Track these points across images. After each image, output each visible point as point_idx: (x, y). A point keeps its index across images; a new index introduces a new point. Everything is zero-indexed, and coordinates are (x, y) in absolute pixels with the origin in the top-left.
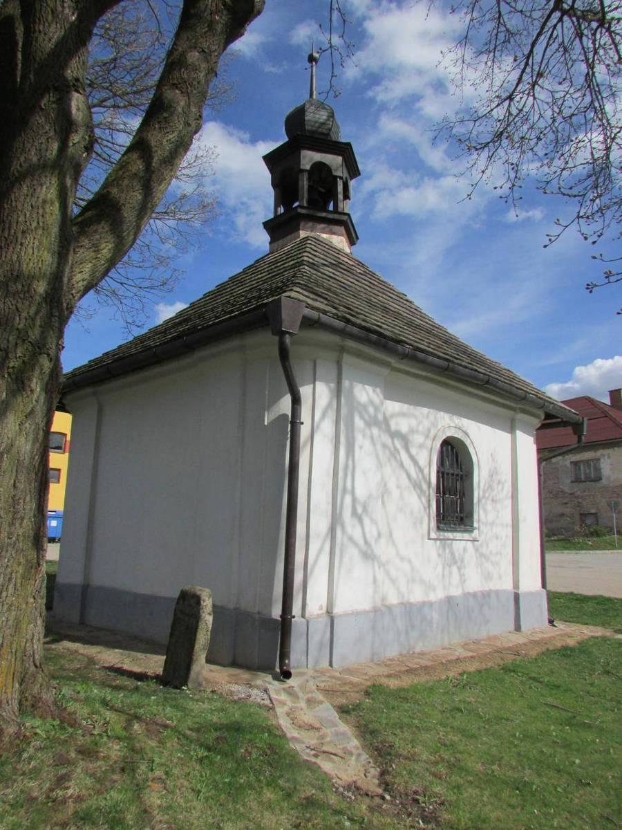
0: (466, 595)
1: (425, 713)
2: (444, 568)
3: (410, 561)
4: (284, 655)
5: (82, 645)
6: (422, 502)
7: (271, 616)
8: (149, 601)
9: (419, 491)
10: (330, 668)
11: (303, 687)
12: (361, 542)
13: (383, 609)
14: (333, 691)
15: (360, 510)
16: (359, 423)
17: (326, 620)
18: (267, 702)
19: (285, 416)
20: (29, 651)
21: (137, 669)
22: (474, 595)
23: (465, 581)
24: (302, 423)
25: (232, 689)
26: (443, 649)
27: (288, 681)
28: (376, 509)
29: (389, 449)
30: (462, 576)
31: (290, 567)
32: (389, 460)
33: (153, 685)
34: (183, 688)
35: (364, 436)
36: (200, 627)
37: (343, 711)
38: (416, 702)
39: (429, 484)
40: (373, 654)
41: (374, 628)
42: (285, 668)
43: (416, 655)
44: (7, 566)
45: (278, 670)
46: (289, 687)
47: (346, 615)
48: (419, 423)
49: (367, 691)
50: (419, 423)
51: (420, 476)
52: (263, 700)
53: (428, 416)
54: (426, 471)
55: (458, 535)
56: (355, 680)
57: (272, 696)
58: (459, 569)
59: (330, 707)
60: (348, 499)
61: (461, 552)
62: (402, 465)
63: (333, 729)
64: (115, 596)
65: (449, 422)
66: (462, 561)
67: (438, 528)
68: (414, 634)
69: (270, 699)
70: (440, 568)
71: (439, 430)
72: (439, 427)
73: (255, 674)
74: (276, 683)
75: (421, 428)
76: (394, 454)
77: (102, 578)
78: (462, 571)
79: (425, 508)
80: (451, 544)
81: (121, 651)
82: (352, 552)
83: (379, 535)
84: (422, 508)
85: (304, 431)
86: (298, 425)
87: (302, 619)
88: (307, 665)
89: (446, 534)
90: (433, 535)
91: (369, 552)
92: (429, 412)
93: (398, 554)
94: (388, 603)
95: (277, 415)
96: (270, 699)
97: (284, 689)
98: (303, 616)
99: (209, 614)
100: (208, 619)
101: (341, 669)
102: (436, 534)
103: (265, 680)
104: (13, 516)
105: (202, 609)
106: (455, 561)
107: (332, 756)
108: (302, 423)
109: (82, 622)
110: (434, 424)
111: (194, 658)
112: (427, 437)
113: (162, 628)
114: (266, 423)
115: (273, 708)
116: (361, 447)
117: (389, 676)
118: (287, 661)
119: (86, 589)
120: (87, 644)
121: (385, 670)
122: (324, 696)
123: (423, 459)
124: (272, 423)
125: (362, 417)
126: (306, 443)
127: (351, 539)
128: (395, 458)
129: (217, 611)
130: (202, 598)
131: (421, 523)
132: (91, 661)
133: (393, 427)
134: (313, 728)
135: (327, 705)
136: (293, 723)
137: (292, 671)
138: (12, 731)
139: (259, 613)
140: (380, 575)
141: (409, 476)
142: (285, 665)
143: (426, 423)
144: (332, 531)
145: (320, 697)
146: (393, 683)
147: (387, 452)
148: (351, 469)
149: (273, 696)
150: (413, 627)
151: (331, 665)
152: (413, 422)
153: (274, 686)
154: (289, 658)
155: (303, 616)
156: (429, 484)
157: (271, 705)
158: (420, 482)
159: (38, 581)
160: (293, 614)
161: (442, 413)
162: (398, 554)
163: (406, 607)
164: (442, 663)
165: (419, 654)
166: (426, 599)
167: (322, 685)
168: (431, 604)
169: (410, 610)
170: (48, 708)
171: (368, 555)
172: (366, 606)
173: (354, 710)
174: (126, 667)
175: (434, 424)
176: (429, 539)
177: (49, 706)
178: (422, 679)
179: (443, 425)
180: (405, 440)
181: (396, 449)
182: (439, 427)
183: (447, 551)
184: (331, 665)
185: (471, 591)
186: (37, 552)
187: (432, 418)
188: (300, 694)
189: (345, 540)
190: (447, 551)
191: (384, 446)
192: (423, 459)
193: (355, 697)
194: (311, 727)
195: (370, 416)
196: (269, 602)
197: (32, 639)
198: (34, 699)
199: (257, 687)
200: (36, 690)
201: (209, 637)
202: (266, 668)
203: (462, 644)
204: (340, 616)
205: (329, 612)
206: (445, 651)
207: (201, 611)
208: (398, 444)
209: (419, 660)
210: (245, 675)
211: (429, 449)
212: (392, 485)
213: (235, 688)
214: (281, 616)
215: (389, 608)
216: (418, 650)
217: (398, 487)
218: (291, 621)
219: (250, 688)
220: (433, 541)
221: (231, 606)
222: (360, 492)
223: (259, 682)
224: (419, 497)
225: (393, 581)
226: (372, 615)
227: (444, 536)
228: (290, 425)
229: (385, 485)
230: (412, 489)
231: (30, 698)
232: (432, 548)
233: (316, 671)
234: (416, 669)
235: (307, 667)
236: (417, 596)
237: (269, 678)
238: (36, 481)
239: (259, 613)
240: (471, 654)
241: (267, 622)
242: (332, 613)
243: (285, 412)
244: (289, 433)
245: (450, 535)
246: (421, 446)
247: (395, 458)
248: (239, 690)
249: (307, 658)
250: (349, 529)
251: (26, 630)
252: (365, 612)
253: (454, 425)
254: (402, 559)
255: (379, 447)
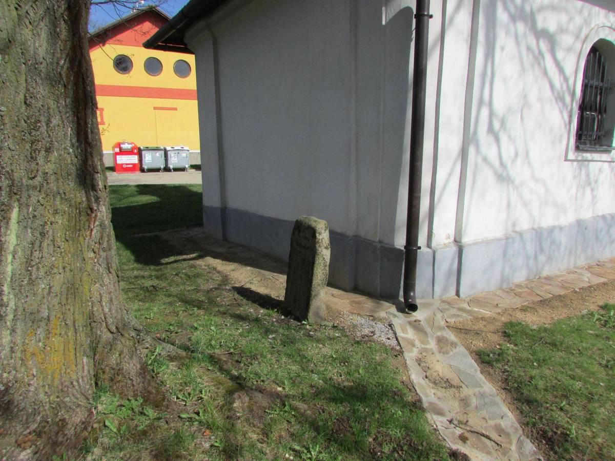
0: (595, 218)
1: (585, 370)
2: (577, 191)
3: (545, 185)
4: (409, 286)
5: (221, 262)
6: (563, 116)
7: (394, 246)
8: (273, 223)
9: (560, 104)
10: (456, 297)
11: (431, 321)
12: (497, 164)
13: (514, 235)
14: (466, 329)
15: (497, 125)
16: (502, 16)
17: (454, 249)
18: (393, 342)
19: (408, 9)
20: (98, 315)
21: (262, 290)
22: (604, 217)
23: (596, 203)
24: (431, 17)
25: (355, 322)
26: (569, 273)
27: (414, 314)
28: (514, 123)
29: (533, 53)
30: (594, 197)
31: (416, 195)
32: (532, 66)
33: (274, 316)
34: (303, 322)
35: (507, 33)
36: (317, 262)
37: (484, 359)
38: (568, 349)
39: (573, 94)
40: (502, 281)
41: (505, 253)
42: (410, 300)
43: (543, 281)
44: (34, 216)
45: (402, 300)
46: (415, 321)
47: (475, 244)
48: (571, 19)
49: (505, 332)
50: (571, 19)
51: (565, 87)
52: (389, 339)
53: (581, 11)
54: (571, 81)
55: (596, 156)
56: (486, 313)
57: (398, 334)
58: (592, 190)
59: (466, 352)
60: (485, 112)
61: (597, 171)
62: (545, 73)
63: (477, 390)
64: (246, 217)
65: (605, 21)
66: (596, 182)
67: (577, 148)
68: (542, 258)
69: (397, 339)
70: (574, 191)
71: (592, 29)
72: (593, 25)
73: (378, 303)
74: (400, 314)
75: (571, 27)
76: (538, 58)
77: (239, 201)
78: (595, 193)
79: (565, 125)
80: (588, 164)
81: (252, 268)
82: (487, 175)
83: (516, 155)
84: (563, 125)
85: (433, 27)
86: (426, 18)
87: (429, 250)
88: (433, 295)
89: (585, 155)
90: (571, 156)
91: (505, 174)
92: (582, 7)
93: (533, 176)
94: (518, 229)
95: (397, 10)
96: (397, 339)
97: (410, 323)
98: (429, 245)
99: (326, 248)
100: (325, 254)
101: (468, 299)
102: (574, 154)
103: (388, 310)
104: (31, 147)
105: (318, 242)
106: (590, 183)
107: (483, 438)
108: (431, 17)
109: (225, 239)
110: (587, 22)
111: (313, 293)
112: (577, 38)
113: (283, 249)
114: (384, 23)
115: (401, 352)
116: (502, 48)
117: (524, 309)
118: (412, 294)
119: (224, 210)
120: (225, 260)
121: (518, 302)
122: (456, 336)
123: (569, 67)
124: (391, 22)
125: (506, 8)
126: (434, 45)
127: (485, 160)
128: (539, 64)
129: (335, 237)
130: (317, 232)
131: (560, 141)
132: (225, 279)
133: (540, 25)
134: (451, 386)
135: (461, 349)
136: (426, 377)
137: (418, 302)
138: (79, 420)
139: (380, 242)
140: (514, 198)
141: (552, 86)
142: (410, 297)
143: (578, 20)
144: (464, 154)
145: (451, 336)
146: (533, 320)
147: (531, 56)
148: (489, 77)
149: (400, 334)
150: (542, 251)
151: (458, 294)
152: (564, 18)
153: (399, 320)
154: (414, 290)
155: (429, 245)
156: (573, 94)
157: (398, 348)
158: (564, 95)
159: (95, 231)
160: (419, 245)
161: (597, 8)
162: (533, 176)
163: (537, 232)
164: (576, 292)
165: (546, 278)
166: (556, 224)
167: (452, 320)
168: (561, 228)
169: (542, 236)
170: (129, 382)
171: (503, 178)
172: (498, 233)
173: (497, 361)
174: (254, 288)
175: (587, 22)
176: (566, 160)
177: (131, 380)
178: (560, 314)
179: (597, 23)
180: (551, 40)
181: (540, 52)
182: (593, 25)
183: (583, 171)
184: (458, 294)
185: (601, 214)
186: (86, 192)
187: (585, 13)
188: (428, 330)
189: (480, 160)
190: (583, 171)
191: (529, 49)
192: (569, 67)
193: (494, 340)
194: (448, 384)
195: (515, 6)
196: (392, 231)
197: (100, 302)
198: (112, 371)
199: (380, 320)
200: (113, 359)
201: (328, 272)
202: (390, 297)
203: (587, 267)
204: (470, 245)
205: (457, 242)
206: (571, 276)
207: (317, 246)
208: (544, 46)
209: (548, 287)
210: (368, 303)
211: (577, 53)
212: (533, 97)
213: (358, 320)
214: (405, 247)
215: (521, 234)
216: (545, 273)
217: (540, 99)
218: (417, 252)
219: (373, 320)
220: (570, 162)
221: (350, 233)
222: (499, 105)
223: (382, 314)
224: (561, 112)
225: (526, 205)
226: (504, 241)
227: (583, 157)
228: (414, 21)
229: (525, 97)
230: (554, 102)
231: (107, 369)
232: (569, 169)
233: (443, 302)
234: (550, 300)
235: (433, 298)
236: (548, 221)
237: (393, 309)
238: (66, 96)
239: (380, 242)
240: (602, 280)
241: (390, 252)
242: (460, 242)
243: (410, 6)
244: (414, 33)
245: (588, 156)
246: (569, 50)
247: (539, 64)
248: (364, 326)
249: (433, 289)
250: (484, 149)
251: (90, 291)
252: (499, 240)
253: (609, 25)
254: (537, 181)
255: (523, 48)
